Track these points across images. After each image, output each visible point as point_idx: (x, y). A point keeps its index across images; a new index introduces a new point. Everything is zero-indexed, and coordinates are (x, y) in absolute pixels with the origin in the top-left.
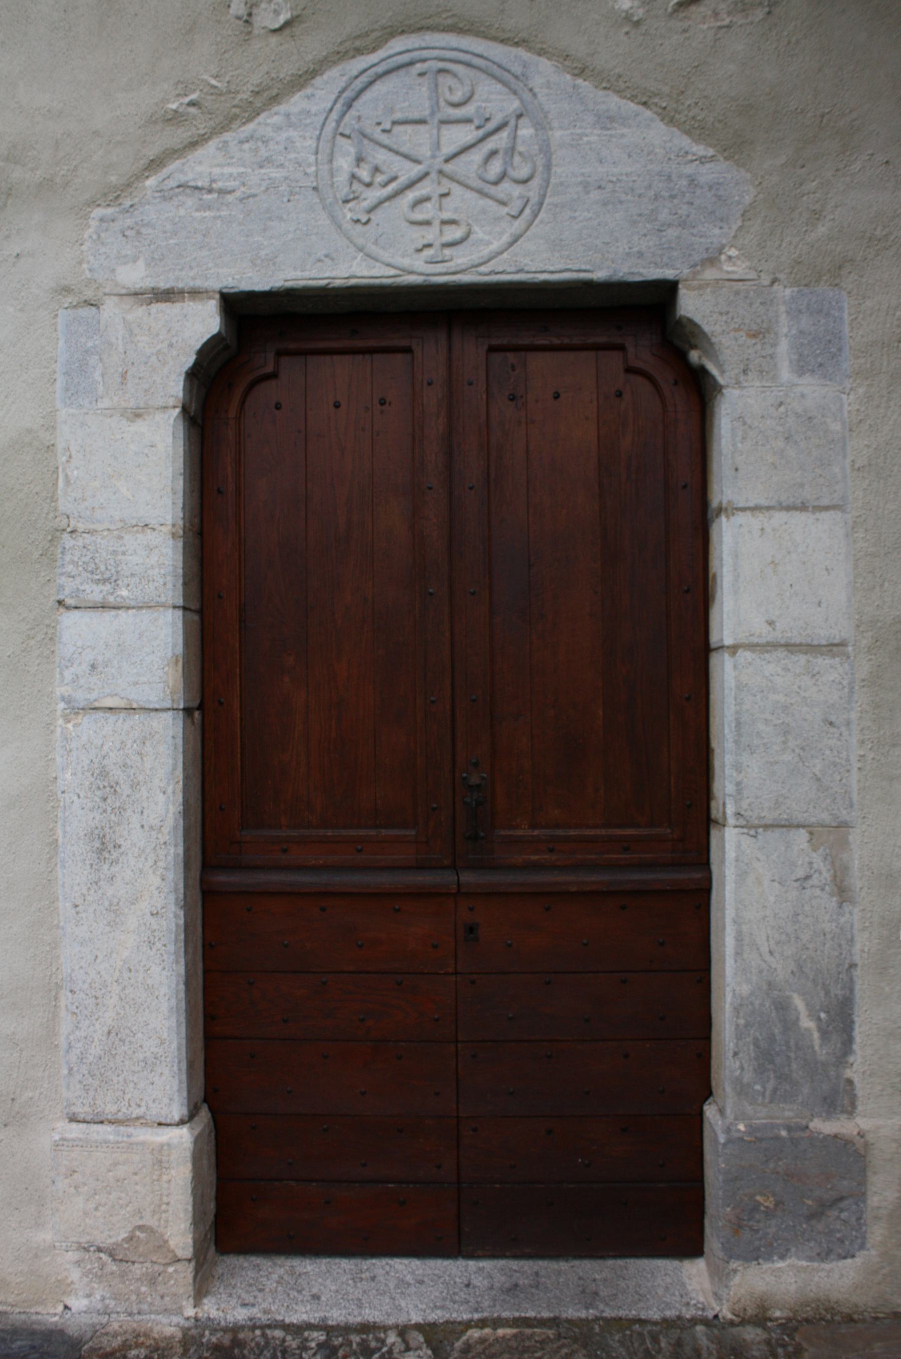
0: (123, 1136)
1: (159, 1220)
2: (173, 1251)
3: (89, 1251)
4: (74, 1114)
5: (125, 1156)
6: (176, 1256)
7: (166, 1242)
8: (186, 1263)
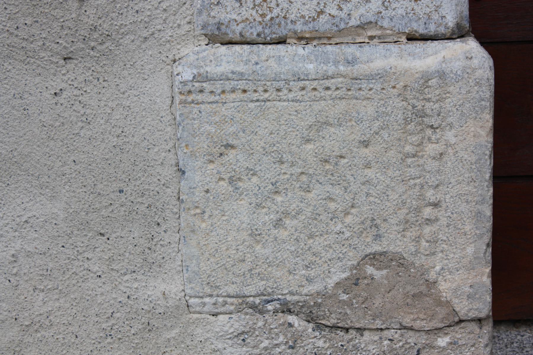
0: (336, 63)
1: (417, 240)
2: (448, 303)
3: (262, 312)
4: (219, 25)
5: (342, 105)
6: (455, 312)
7: (432, 284)
8: (473, 326)
